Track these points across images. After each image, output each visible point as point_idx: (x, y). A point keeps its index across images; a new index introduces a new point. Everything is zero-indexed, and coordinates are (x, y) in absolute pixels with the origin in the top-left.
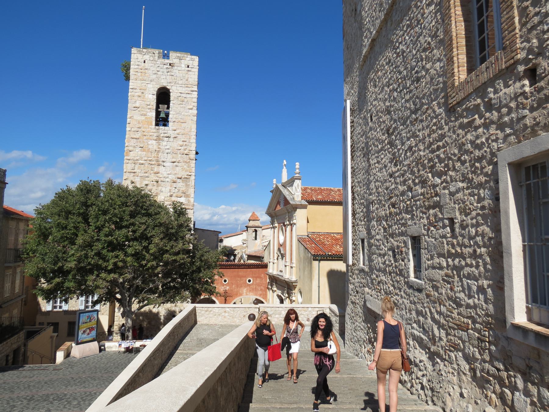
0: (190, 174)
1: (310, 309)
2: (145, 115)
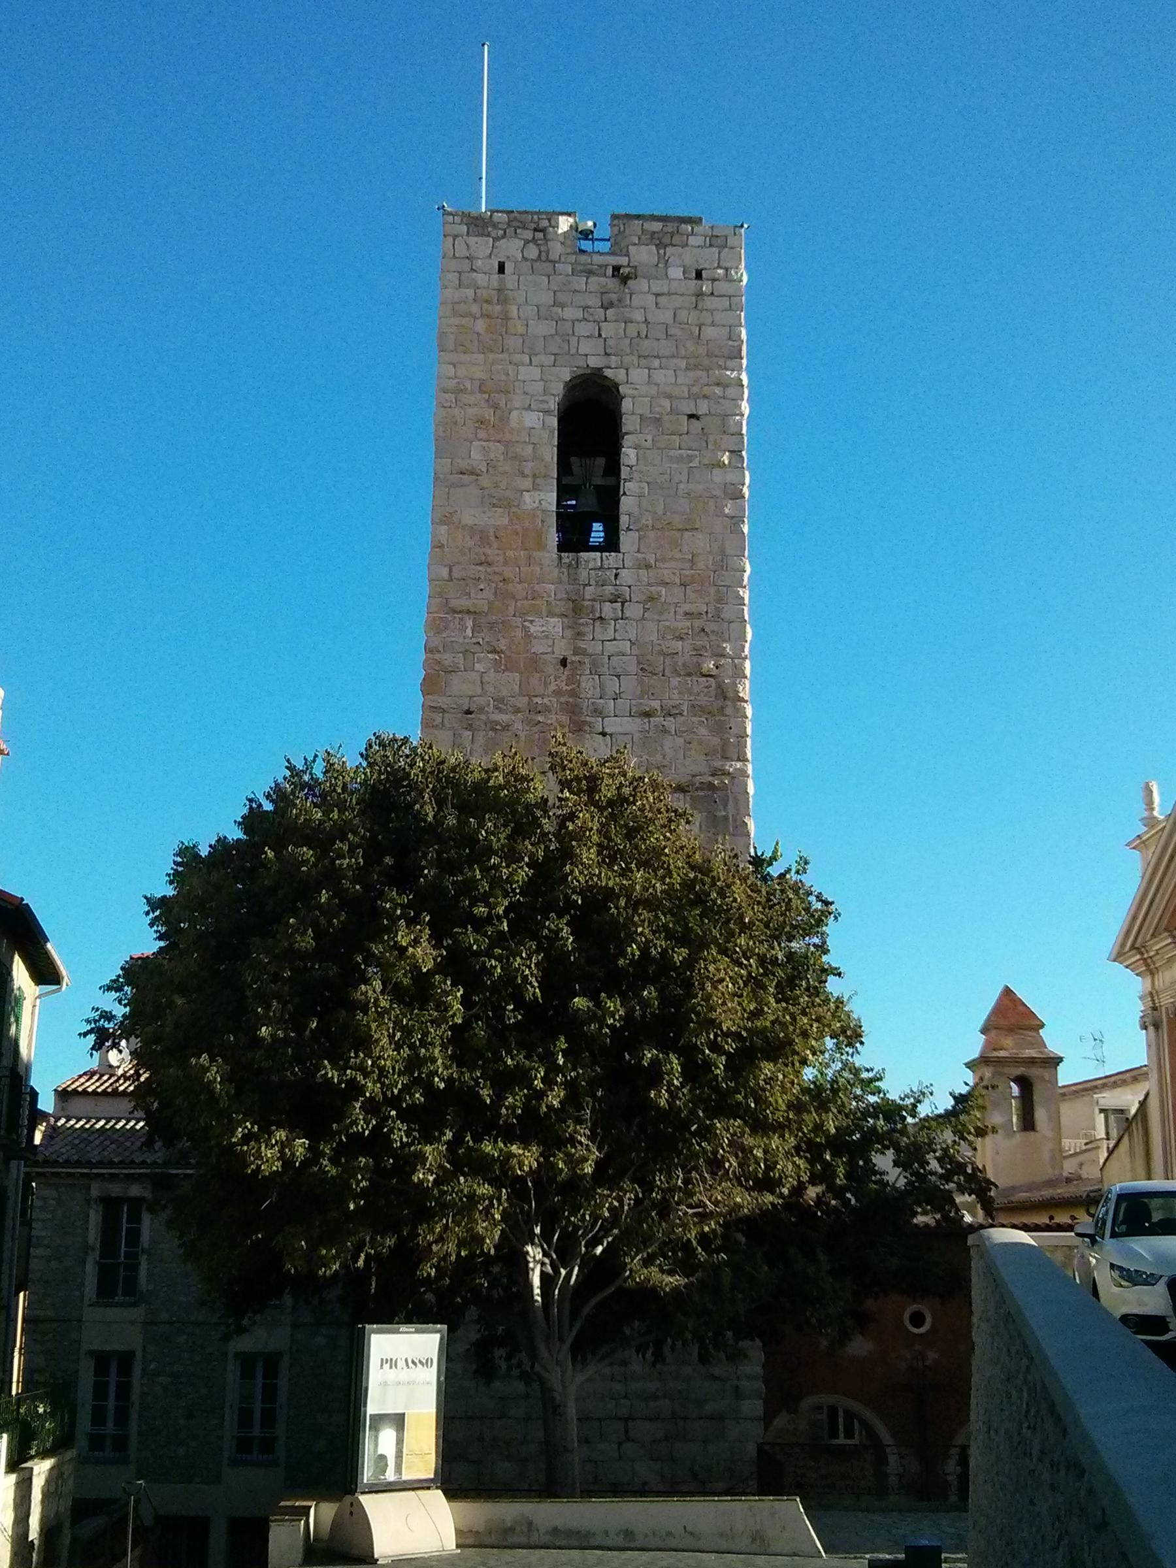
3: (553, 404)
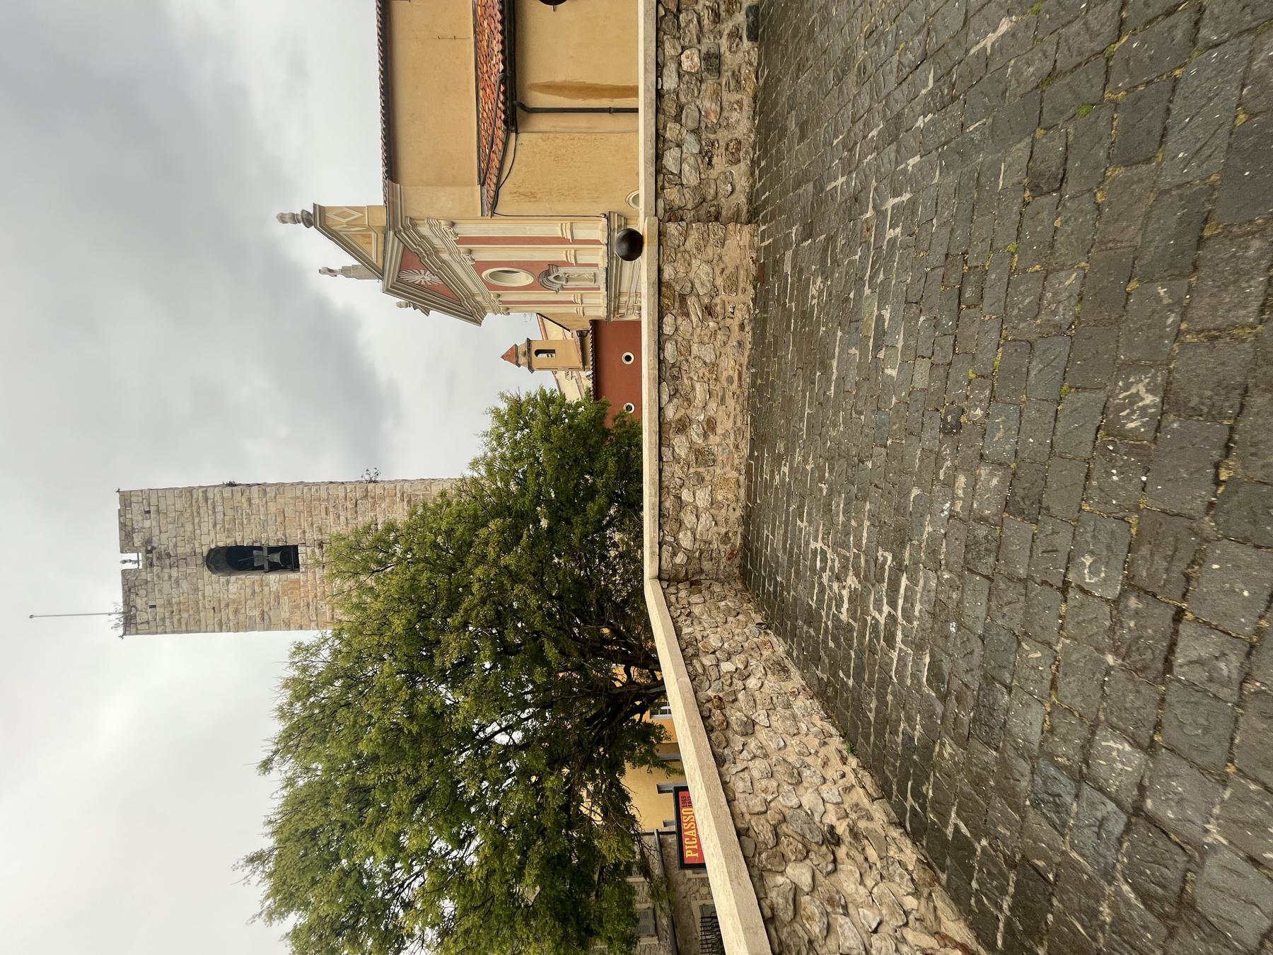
0: (399, 495)
1: (670, 83)
2: (278, 598)
3: (223, 579)
